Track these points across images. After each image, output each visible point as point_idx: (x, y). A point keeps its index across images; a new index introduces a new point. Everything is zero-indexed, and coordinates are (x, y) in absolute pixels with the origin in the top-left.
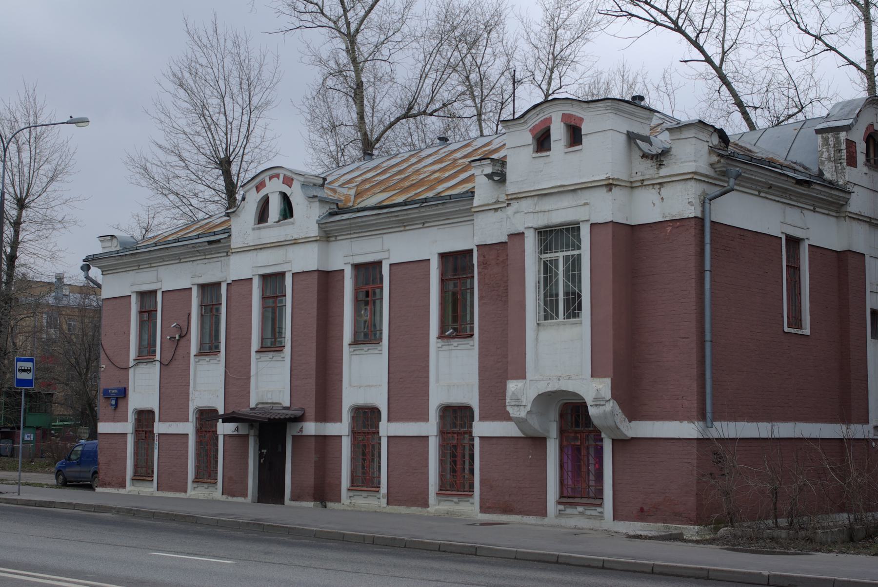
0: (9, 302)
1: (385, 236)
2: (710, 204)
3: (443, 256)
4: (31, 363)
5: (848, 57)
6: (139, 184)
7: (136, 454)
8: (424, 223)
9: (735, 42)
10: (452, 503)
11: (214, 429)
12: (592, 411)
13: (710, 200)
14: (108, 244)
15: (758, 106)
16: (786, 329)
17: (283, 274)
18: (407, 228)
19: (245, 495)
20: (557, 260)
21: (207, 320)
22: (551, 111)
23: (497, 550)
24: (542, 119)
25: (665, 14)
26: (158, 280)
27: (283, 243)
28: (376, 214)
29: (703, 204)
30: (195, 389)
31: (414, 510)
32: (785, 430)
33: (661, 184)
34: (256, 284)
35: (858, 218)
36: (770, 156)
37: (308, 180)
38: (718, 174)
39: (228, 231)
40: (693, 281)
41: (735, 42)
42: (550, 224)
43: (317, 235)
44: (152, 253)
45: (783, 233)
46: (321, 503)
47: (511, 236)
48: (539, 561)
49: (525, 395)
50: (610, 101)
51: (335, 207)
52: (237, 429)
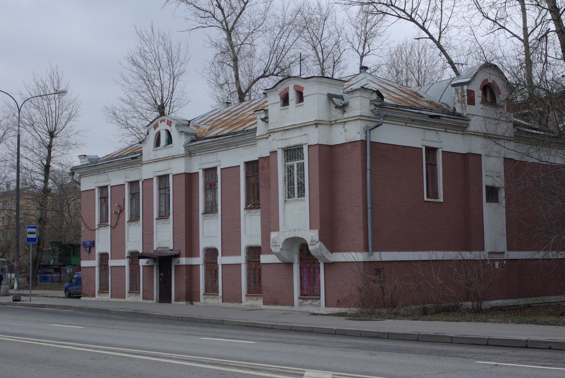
0: (46, 192)
1: (218, 153)
2: (370, 132)
3: (247, 164)
4: (35, 229)
5: (513, 32)
6: (112, 122)
7: (100, 278)
8: (237, 145)
9: (447, 26)
10: (253, 300)
11: (138, 263)
12: (310, 248)
13: (370, 130)
14: (83, 160)
15: (463, 63)
16: (426, 199)
17: (168, 175)
18: (229, 148)
19: (152, 299)
20: (293, 166)
21: (134, 201)
22: (288, 84)
23: (231, 321)
24: (285, 88)
25: (404, 11)
26: (109, 180)
27: (167, 158)
28: (212, 141)
29: (366, 132)
30: (128, 241)
31: (235, 305)
32: (439, 255)
33: (344, 122)
34: (155, 181)
35: (476, 134)
36: (432, 100)
37: (179, 122)
38: (376, 116)
39: (141, 152)
40: (361, 175)
41: (447, 26)
42: (289, 146)
43: (184, 153)
44: (104, 165)
45: (423, 145)
46: (190, 302)
47: (271, 152)
48: (247, 326)
49: (279, 240)
50: (315, 78)
51: (195, 137)
52: (148, 262)
